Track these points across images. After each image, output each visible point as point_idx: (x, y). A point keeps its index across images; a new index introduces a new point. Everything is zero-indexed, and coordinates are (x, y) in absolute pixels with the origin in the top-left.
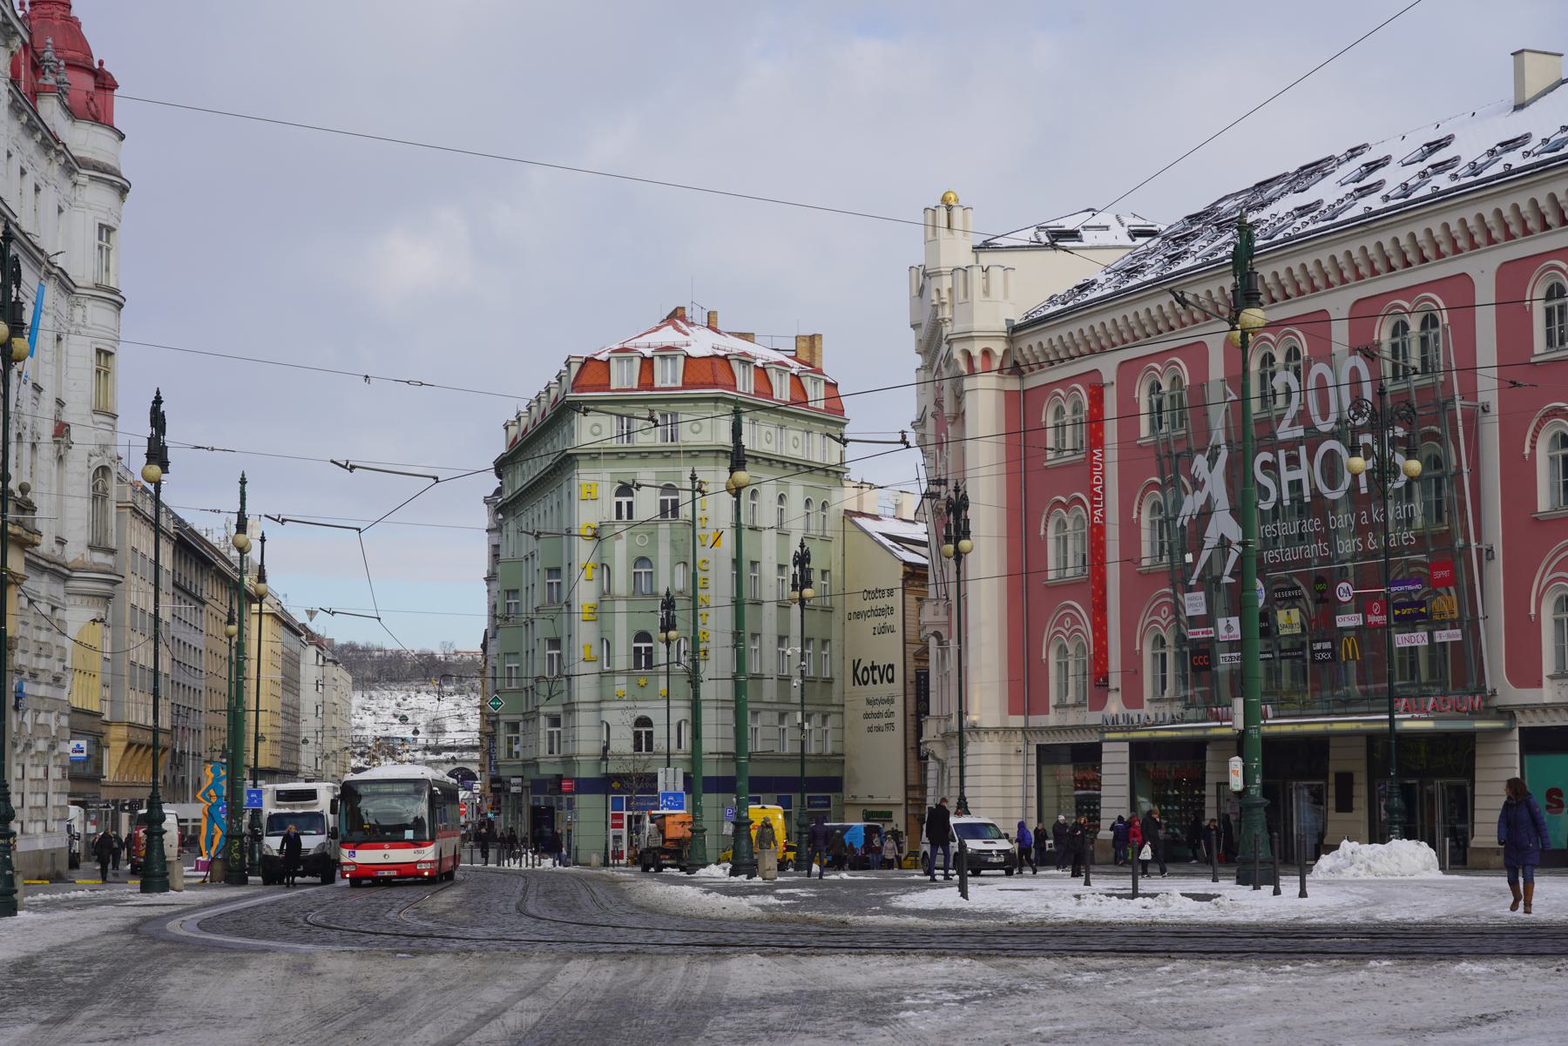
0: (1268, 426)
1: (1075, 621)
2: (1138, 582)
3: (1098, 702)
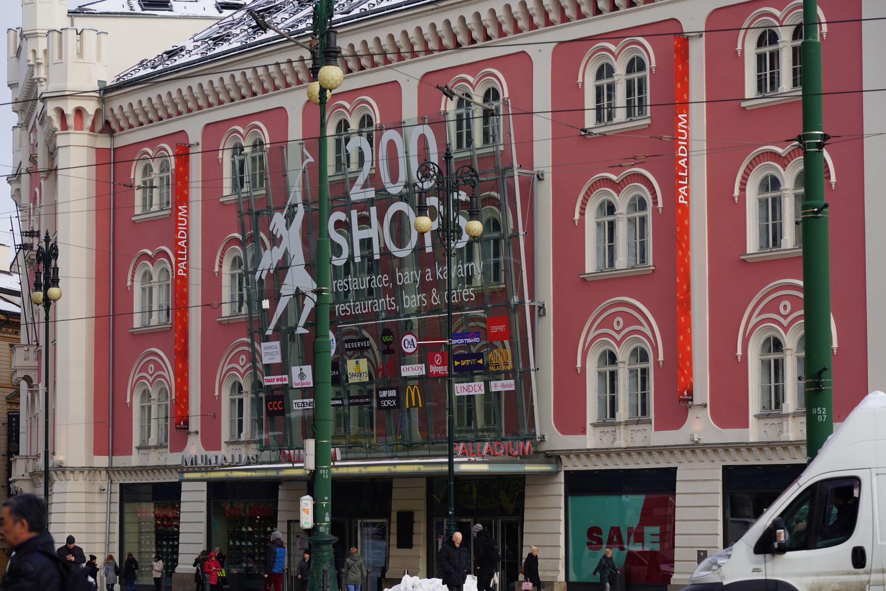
0: (343, 187)
1: (158, 367)
2: (736, 277)
3: (179, 445)
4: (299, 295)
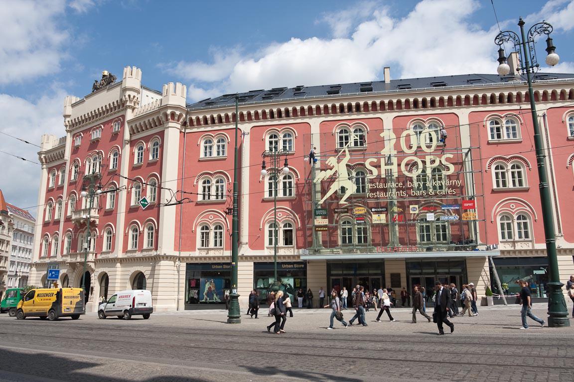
4: (343, 189)
